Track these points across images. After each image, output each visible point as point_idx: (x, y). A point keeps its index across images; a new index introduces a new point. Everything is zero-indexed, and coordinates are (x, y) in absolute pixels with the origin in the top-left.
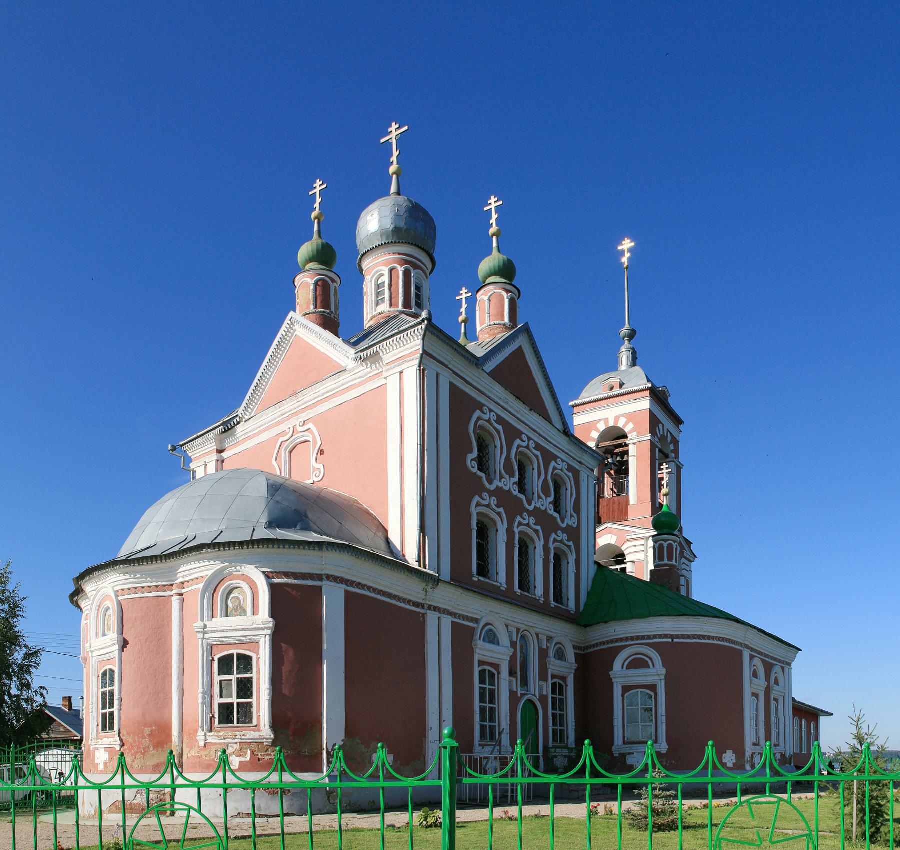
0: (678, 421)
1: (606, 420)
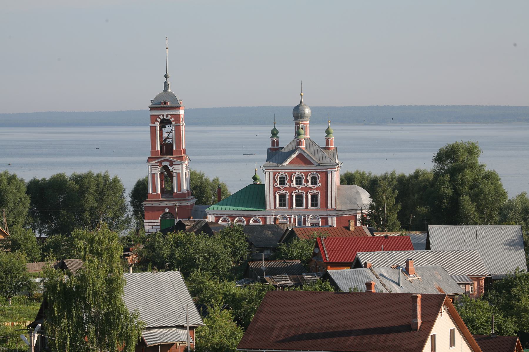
1: (163, 115)
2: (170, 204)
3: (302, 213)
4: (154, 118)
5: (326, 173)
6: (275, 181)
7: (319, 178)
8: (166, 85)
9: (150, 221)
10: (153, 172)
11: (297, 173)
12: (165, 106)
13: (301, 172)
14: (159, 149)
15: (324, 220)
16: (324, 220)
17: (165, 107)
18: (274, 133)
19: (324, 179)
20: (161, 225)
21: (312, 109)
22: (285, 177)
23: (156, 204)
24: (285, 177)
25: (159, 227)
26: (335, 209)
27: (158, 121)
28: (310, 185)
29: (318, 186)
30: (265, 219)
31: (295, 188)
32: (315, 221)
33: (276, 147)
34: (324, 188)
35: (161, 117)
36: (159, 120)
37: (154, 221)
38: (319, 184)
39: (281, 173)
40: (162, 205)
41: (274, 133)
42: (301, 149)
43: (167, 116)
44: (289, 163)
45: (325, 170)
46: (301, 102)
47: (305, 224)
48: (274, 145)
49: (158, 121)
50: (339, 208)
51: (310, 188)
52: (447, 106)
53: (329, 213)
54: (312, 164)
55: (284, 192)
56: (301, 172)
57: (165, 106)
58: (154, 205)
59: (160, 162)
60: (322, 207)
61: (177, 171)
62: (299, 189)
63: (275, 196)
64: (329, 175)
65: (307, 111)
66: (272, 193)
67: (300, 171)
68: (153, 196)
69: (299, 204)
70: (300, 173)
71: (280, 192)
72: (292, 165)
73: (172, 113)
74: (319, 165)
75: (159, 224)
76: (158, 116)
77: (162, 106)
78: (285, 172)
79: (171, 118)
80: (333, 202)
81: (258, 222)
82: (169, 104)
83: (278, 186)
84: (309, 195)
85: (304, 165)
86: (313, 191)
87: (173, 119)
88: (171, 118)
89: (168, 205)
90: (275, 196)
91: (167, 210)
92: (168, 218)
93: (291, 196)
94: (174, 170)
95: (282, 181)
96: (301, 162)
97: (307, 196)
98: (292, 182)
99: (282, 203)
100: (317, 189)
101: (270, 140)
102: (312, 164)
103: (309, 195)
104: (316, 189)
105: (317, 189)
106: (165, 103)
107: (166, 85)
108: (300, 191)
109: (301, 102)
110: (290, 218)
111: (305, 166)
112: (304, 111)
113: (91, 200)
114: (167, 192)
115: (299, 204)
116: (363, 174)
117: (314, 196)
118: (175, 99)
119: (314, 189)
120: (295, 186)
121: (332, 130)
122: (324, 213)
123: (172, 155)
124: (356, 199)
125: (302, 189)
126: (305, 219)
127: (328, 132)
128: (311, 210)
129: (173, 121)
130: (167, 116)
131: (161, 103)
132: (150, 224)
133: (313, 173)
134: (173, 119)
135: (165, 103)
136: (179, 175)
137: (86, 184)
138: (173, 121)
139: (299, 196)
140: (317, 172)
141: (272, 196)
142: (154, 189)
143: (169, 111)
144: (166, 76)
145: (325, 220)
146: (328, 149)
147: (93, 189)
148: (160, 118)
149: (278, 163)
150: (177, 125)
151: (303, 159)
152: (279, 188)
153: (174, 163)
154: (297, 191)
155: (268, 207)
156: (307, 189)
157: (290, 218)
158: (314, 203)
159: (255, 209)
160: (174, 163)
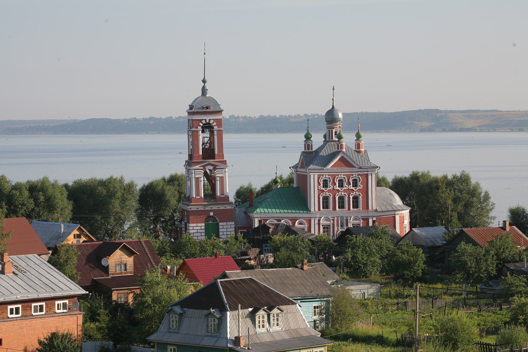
0: (220, 112)
1: (205, 120)
2: (215, 208)
3: (344, 215)
4: (192, 124)
5: (367, 176)
6: (319, 184)
7: (360, 180)
8: (204, 91)
9: (195, 225)
10: (197, 176)
11: (340, 176)
12: (207, 110)
13: (344, 175)
14: (201, 154)
15: (365, 222)
16: (365, 222)
17: (208, 112)
18: (308, 137)
19: (365, 181)
20: (205, 229)
21: (343, 114)
22: (358, 179)
23: (201, 208)
24: (358, 179)
25: (204, 231)
26: (376, 211)
27: (200, 126)
28: (352, 188)
29: (360, 188)
30: (310, 220)
31: (338, 190)
32: (357, 222)
33: (310, 151)
34: (365, 190)
35: (204, 122)
36: (201, 124)
37: (199, 225)
38: (360, 186)
39: (324, 176)
40: (207, 209)
41: (308, 137)
42: (343, 152)
43: (210, 120)
44: (332, 166)
45: (366, 173)
46: (333, 107)
47: (347, 225)
48: (308, 149)
49: (200, 126)
50: (379, 209)
51: (352, 190)
52: (262, 118)
53: (370, 214)
54: (353, 167)
55: (328, 194)
56: (344, 175)
57: (207, 110)
58: (220, 208)
59: (204, 167)
60: (363, 209)
61: (221, 175)
62: (341, 192)
63: (319, 198)
64: (370, 177)
65: (340, 115)
66: (316, 195)
67: (343, 173)
68: (196, 200)
69: (342, 206)
70: (342, 176)
71: (324, 195)
72: (335, 168)
73: (214, 118)
74: (361, 168)
75: (203, 228)
76: (201, 121)
77: (204, 110)
78: (329, 175)
79: (213, 123)
80: (373, 204)
81: (302, 224)
82: (212, 109)
83: (322, 188)
84: (351, 197)
85: (346, 168)
86: (354, 193)
87: (215, 124)
88: (213, 123)
89: (213, 209)
90: (319, 198)
91: (212, 214)
92: (211, 222)
93: (334, 198)
94: (218, 174)
95: (325, 185)
96: (343, 165)
97: (349, 198)
98: (335, 184)
99: (326, 206)
100: (358, 191)
101: (304, 143)
102: (353, 167)
103: (351, 197)
104: (357, 191)
105: (358, 191)
106: (207, 108)
107: (204, 91)
108: (343, 193)
109: (333, 107)
110: (333, 220)
111: (347, 169)
112: (338, 115)
113: (116, 204)
114: (211, 195)
115: (342, 206)
116: (121, 181)
117: (356, 198)
118: (217, 104)
119: (356, 191)
120: (338, 188)
121: (362, 134)
122: (365, 214)
123: (214, 159)
124: (391, 200)
125: (344, 191)
126: (347, 220)
127: (358, 136)
128: (353, 212)
129: (215, 125)
130: (210, 120)
131: (203, 108)
132: (195, 228)
133: (355, 175)
134: (215, 124)
135: (207, 108)
136: (222, 179)
137: (111, 189)
138: (215, 125)
139: (341, 199)
140: (358, 175)
141: (316, 199)
142: (198, 194)
143: (210, 115)
144: (204, 81)
145: (366, 220)
146: (359, 152)
147: (119, 194)
148: (202, 123)
149: (321, 166)
150: (219, 129)
151: (345, 162)
152: (323, 191)
153: (217, 167)
154: (340, 193)
155: (312, 210)
156: (349, 191)
157: (333, 220)
158: (356, 206)
159: (301, 212)
160: (217, 167)
